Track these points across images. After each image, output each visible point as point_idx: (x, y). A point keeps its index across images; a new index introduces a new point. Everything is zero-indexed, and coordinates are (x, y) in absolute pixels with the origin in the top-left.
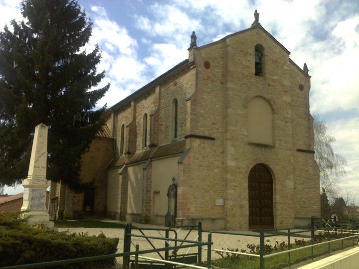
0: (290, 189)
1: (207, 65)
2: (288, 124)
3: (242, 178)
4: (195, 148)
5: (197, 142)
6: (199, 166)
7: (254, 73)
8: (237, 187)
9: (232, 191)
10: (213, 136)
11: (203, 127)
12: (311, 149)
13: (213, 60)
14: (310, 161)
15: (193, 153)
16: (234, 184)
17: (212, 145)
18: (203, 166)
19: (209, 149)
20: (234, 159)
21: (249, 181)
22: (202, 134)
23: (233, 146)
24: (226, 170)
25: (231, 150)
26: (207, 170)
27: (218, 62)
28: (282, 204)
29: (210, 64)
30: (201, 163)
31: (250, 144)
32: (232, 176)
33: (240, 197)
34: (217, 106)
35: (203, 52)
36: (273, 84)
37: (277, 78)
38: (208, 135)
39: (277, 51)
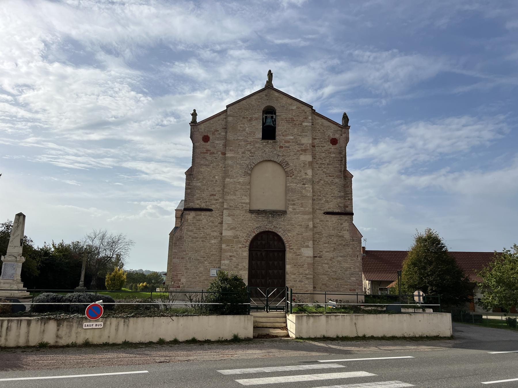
0: (308, 257)
1: (206, 139)
2: (306, 186)
3: (240, 248)
4: (189, 221)
6: (192, 238)
9: (227, 262)
10: (212, 207)
13: (213, 133)
16: (231, 254)
18: (197, 238)
19: (205, 220)
20: (231, 229)
22: (197, 206)
25: (227, 220)
27: (219, 134)
28: (295, 274)
31: (251, 212)
32: (227, 246)
34: (217, 177)
38: (205, 207)
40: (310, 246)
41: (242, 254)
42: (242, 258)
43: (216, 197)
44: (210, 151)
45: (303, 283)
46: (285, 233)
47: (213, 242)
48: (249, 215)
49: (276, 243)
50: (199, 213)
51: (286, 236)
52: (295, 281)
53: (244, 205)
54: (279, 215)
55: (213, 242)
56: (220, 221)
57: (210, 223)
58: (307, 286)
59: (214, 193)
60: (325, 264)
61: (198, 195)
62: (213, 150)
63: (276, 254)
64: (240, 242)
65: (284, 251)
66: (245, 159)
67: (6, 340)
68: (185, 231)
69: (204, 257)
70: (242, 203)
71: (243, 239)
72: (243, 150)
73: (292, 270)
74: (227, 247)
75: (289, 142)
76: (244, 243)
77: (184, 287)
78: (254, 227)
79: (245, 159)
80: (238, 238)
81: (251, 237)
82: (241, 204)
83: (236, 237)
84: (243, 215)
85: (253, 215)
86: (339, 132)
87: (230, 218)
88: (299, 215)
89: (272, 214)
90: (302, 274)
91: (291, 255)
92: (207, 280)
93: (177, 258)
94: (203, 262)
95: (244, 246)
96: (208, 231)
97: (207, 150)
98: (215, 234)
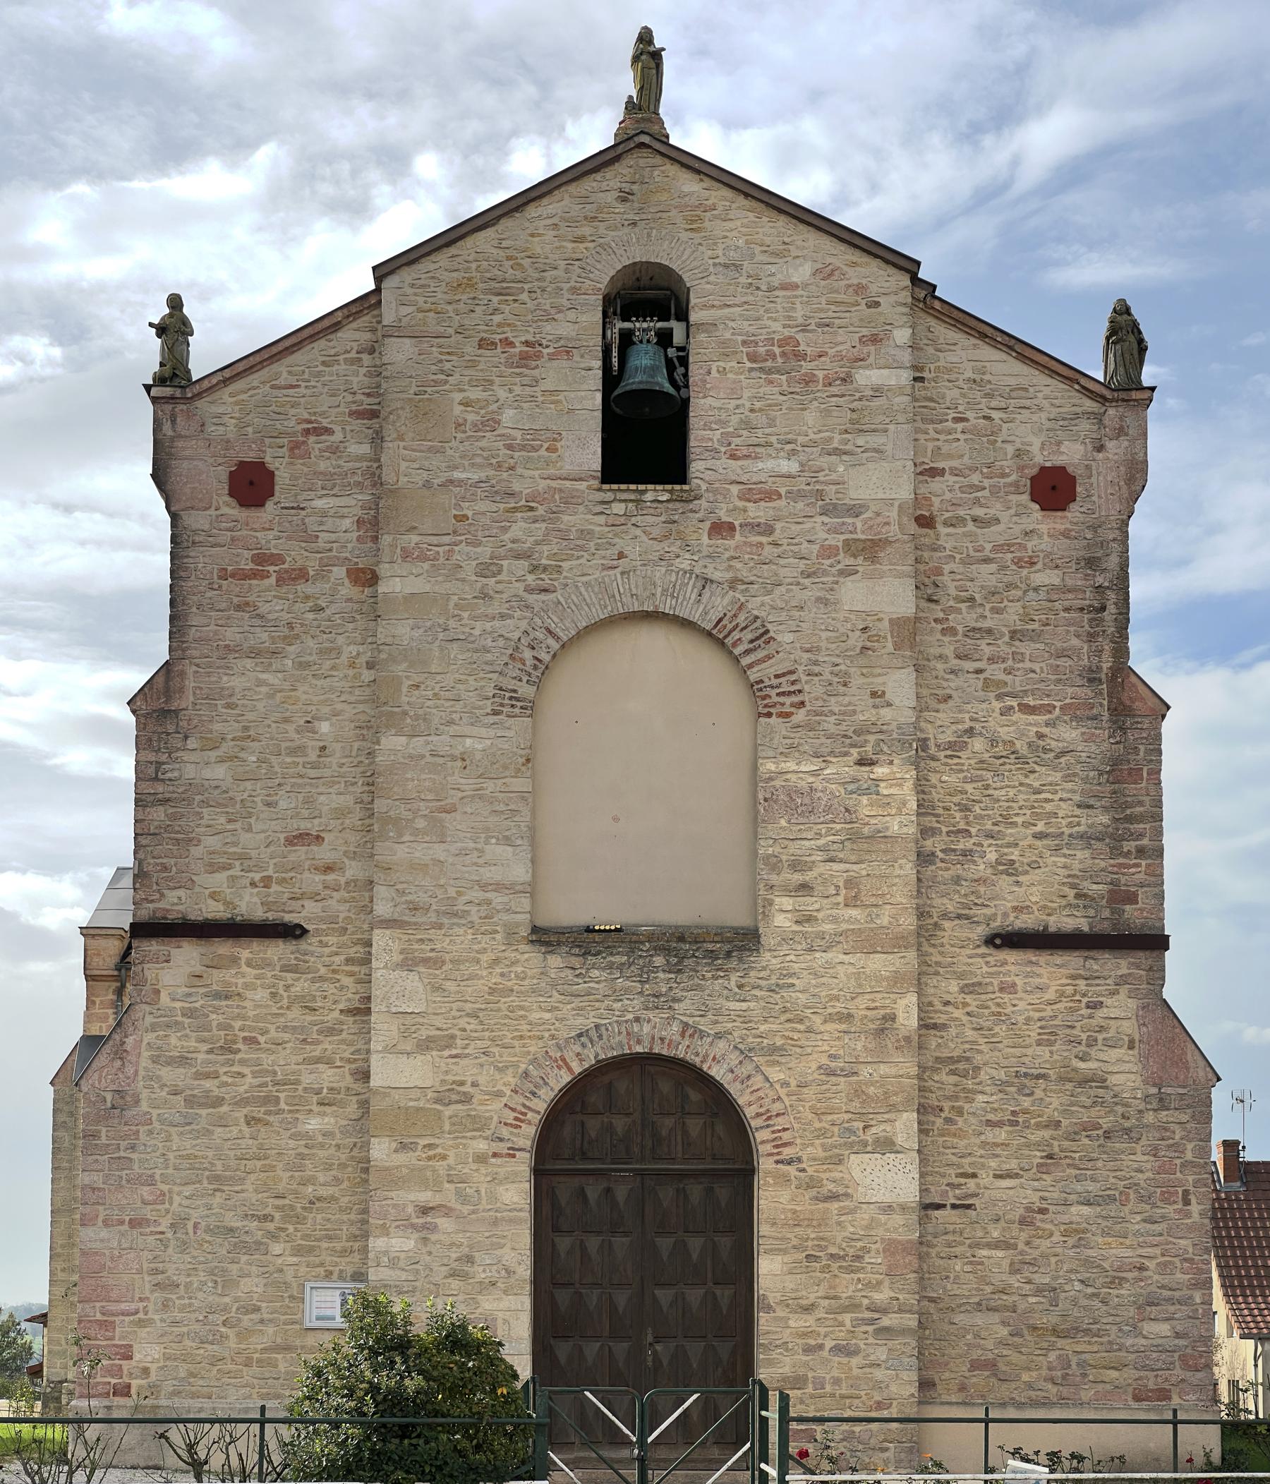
0: (888, 1209)
1: (252, 485)
2: (880, 771)
3: (481, 1159)
4: (164, 998)
5: (187, 954)
6: (190, 1102)
7: (596, 463)
8: (447, 1211)
9: (401, 1244)
11: (228, 867)
12: (1134, 916)
13: (294, 447)
14: (1121, 1009)
15: (153, 1028)
16: (425, 1197)
17: (286, 969)
18: (219, 1101)
19: (261, 995)
20: (425, 1046)
21: (540, 1173)
22: (213, 910)
23: (409, 963)
24: (365, 1108)
25: (400, 991)
26: (250, 1121)
28: (808, 1309)
29: (271, 475)
30: (208, 1084)
32: (403, 1147)
33: (464, 1276)
34: (325, 727)
35: (223, 410)
36: (758, 512)
37: (791, 466)
39: (801, 273)
40: (900, 1140)
41: (493, 1197)
43: (324, 853)
44: (276, 559)
45: (855, 1361)
47: (313, 1124)
48: (530, 958)
49: (695, 1126)
50: (223, 948)
53: (498, 899)
54: (712, 955)
55: (313, 1124)
56: (350, 998)
57: (295, 1014)
58: (879, 1374)
59: (313, 827)
60: (996, 1245)
61: (212, 842)
62: (296, 555)
64: (477, 1124)
66: (496, 608)
68: (144, 1062)
69: (267, 1218)
70: (484, 887)
71: (497, 1105)
72: (485, 552)
74: (402, 1158)
75: (771, 495)
77: (154, 1389)
78: (564, 1034)
79: (496, 608)
80: (467, 1099)
82: (476, 894)
83: (454, 1094)
84: (496, 961)
85: (555, 961)
86: (1085, 426)
87: (413, 981)
88: (835, 956)
89: (666, 951)
90: (853, 1307)
92: (287, 1348)
93: (106, 1223)
94: (259, 1247)
96: (285, 1060)
97: (261, 559)
98: (327, 1077)
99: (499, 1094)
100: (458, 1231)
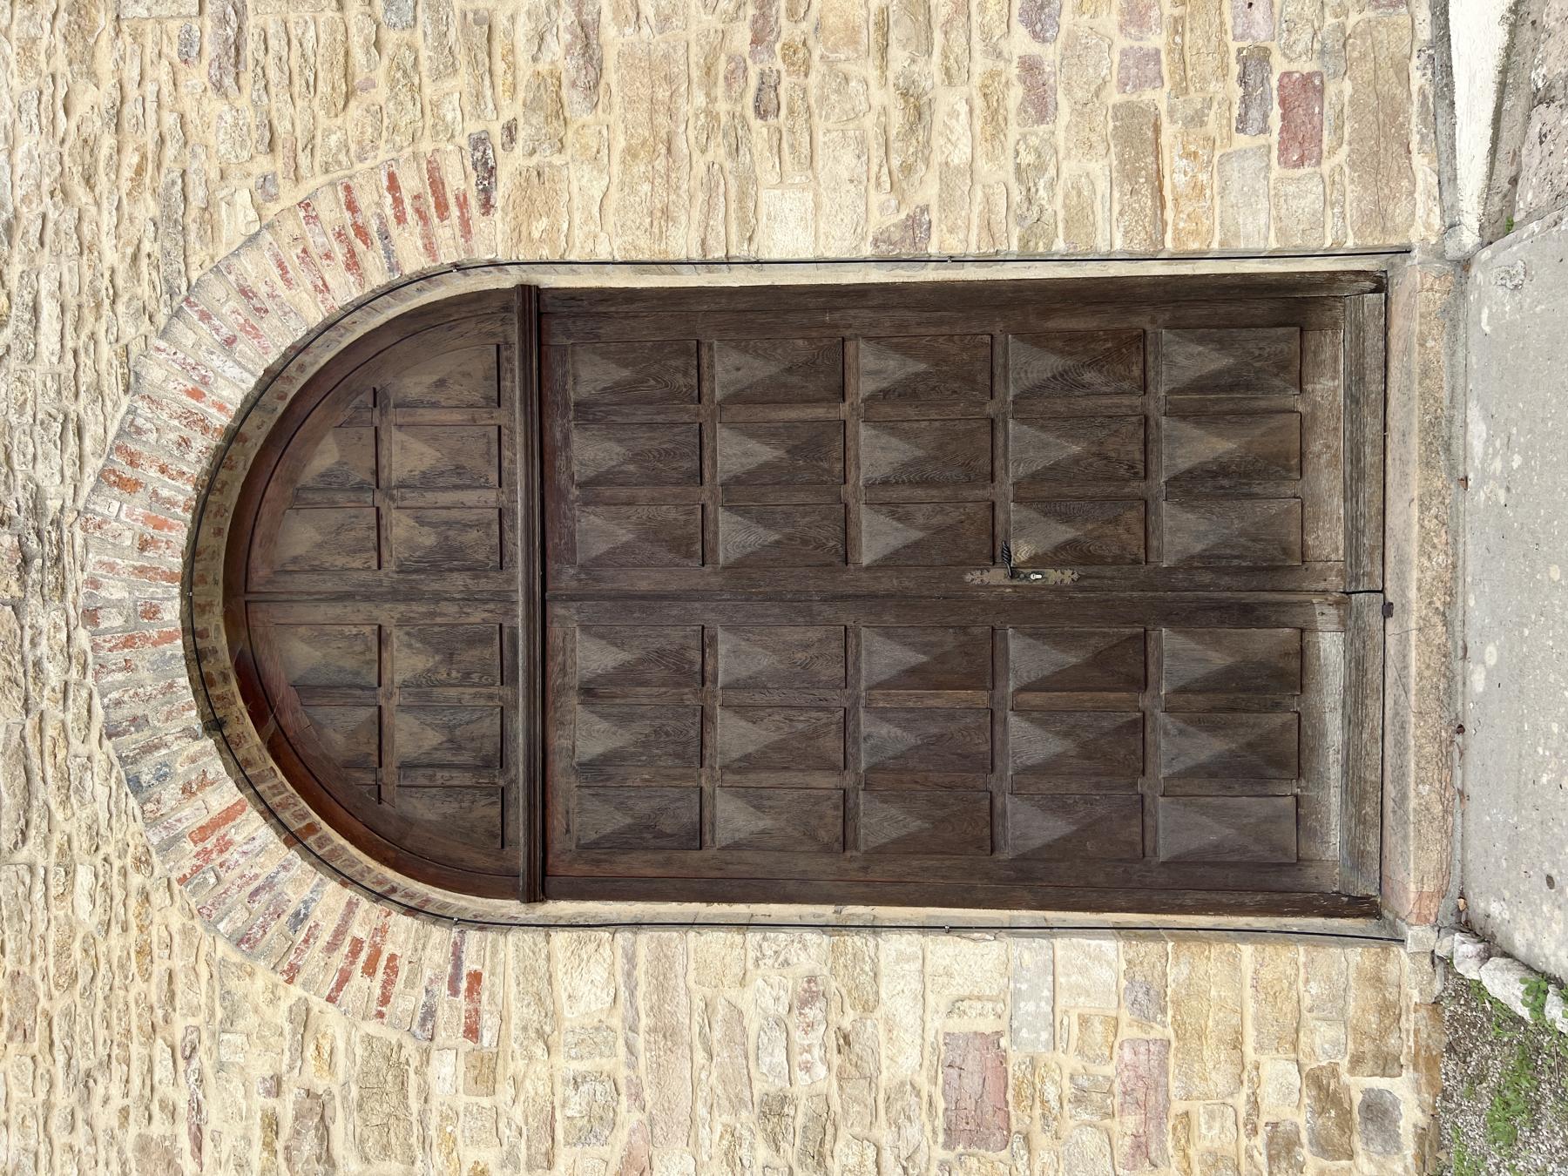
3: (484, 1073)
28: (917, 107)
41: (594, 1037)
42: (666, 1032)
46: (219, 294)
49: (408, 455)
51: (256, 268)
52: (1040, 105)
63: (589, 452)
64: (388, 1077)
65: (539, 323)
67: (631, 959)
71: (332, 1021)
73: (839, 163)
76: (407, 1002)
81: (300, 881)
91: (583, 183)
95: (452, 1011)
99: (303, 1019)
100: (692, 1140)
